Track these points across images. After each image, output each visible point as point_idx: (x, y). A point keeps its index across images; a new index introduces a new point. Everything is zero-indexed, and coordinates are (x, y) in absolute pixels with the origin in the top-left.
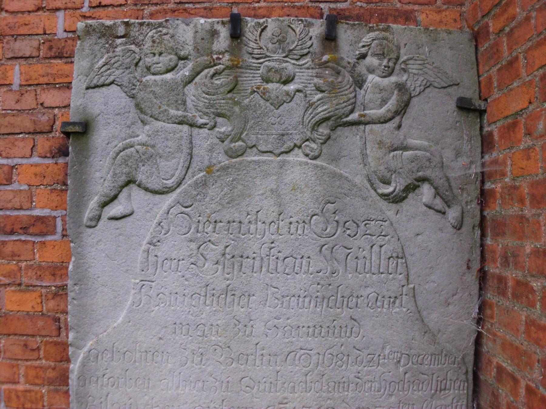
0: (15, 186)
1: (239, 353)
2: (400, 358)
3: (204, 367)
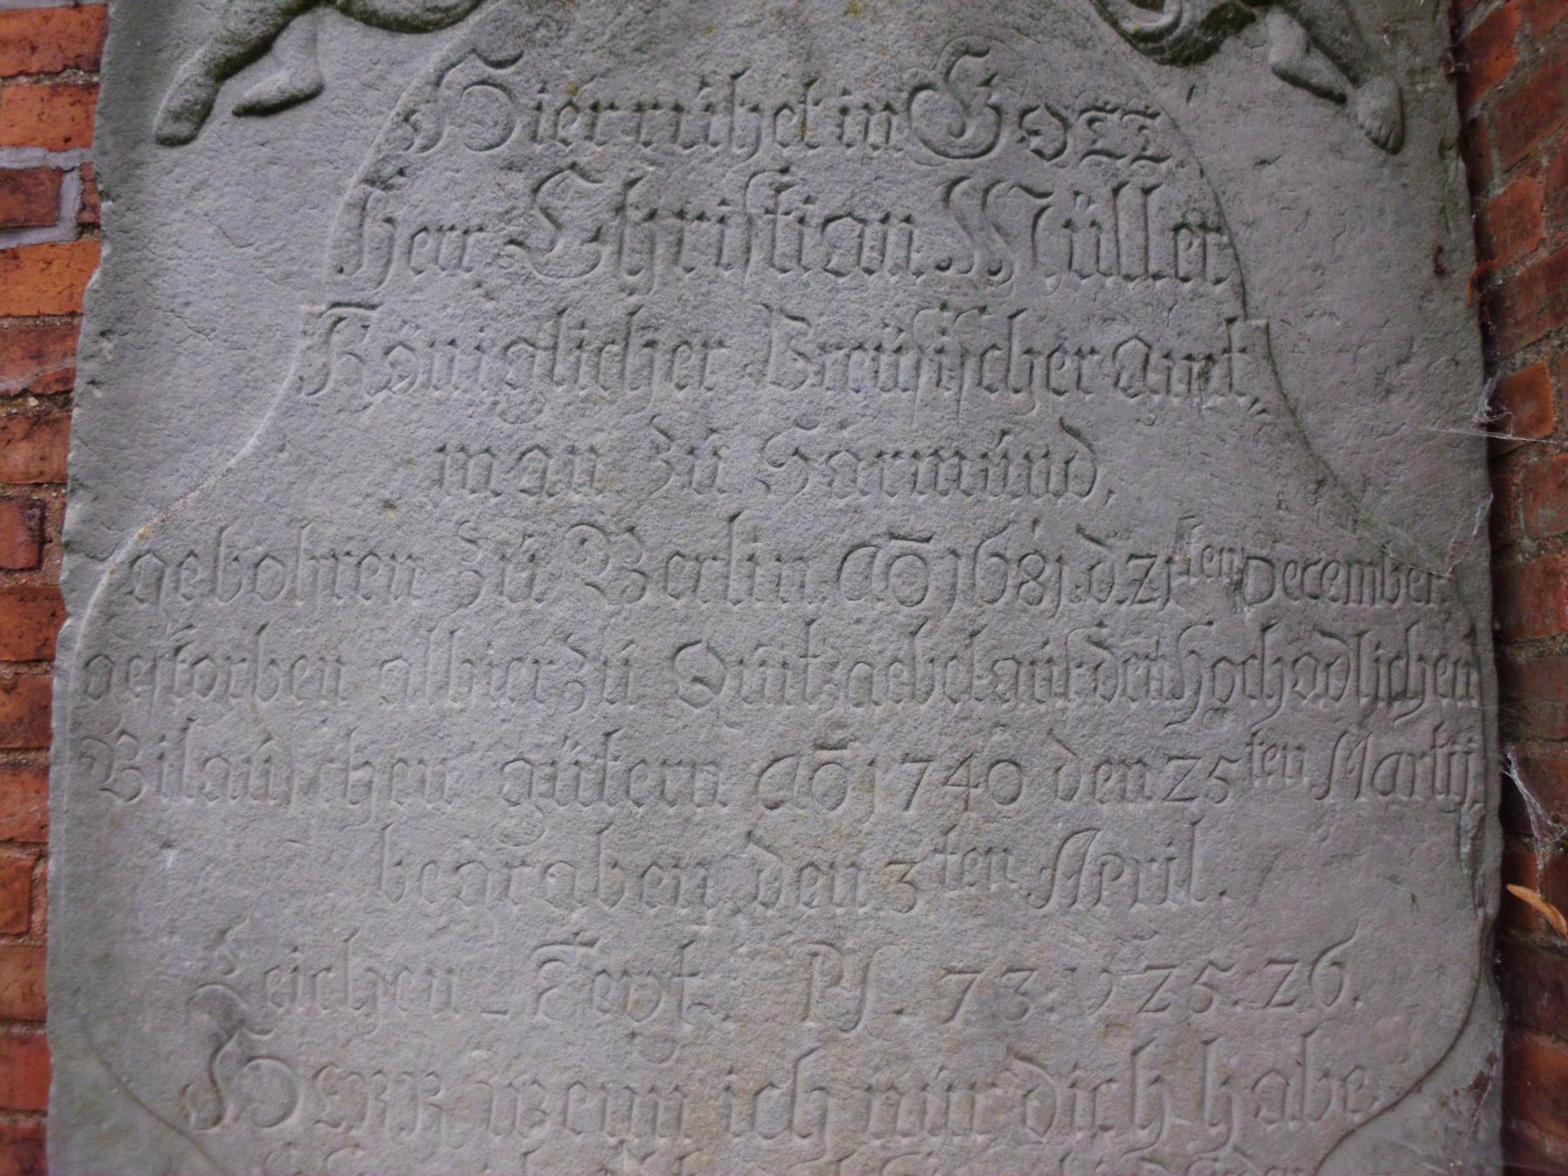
1: (666, 551)
2: (1242, 571)
3: (539, 606)
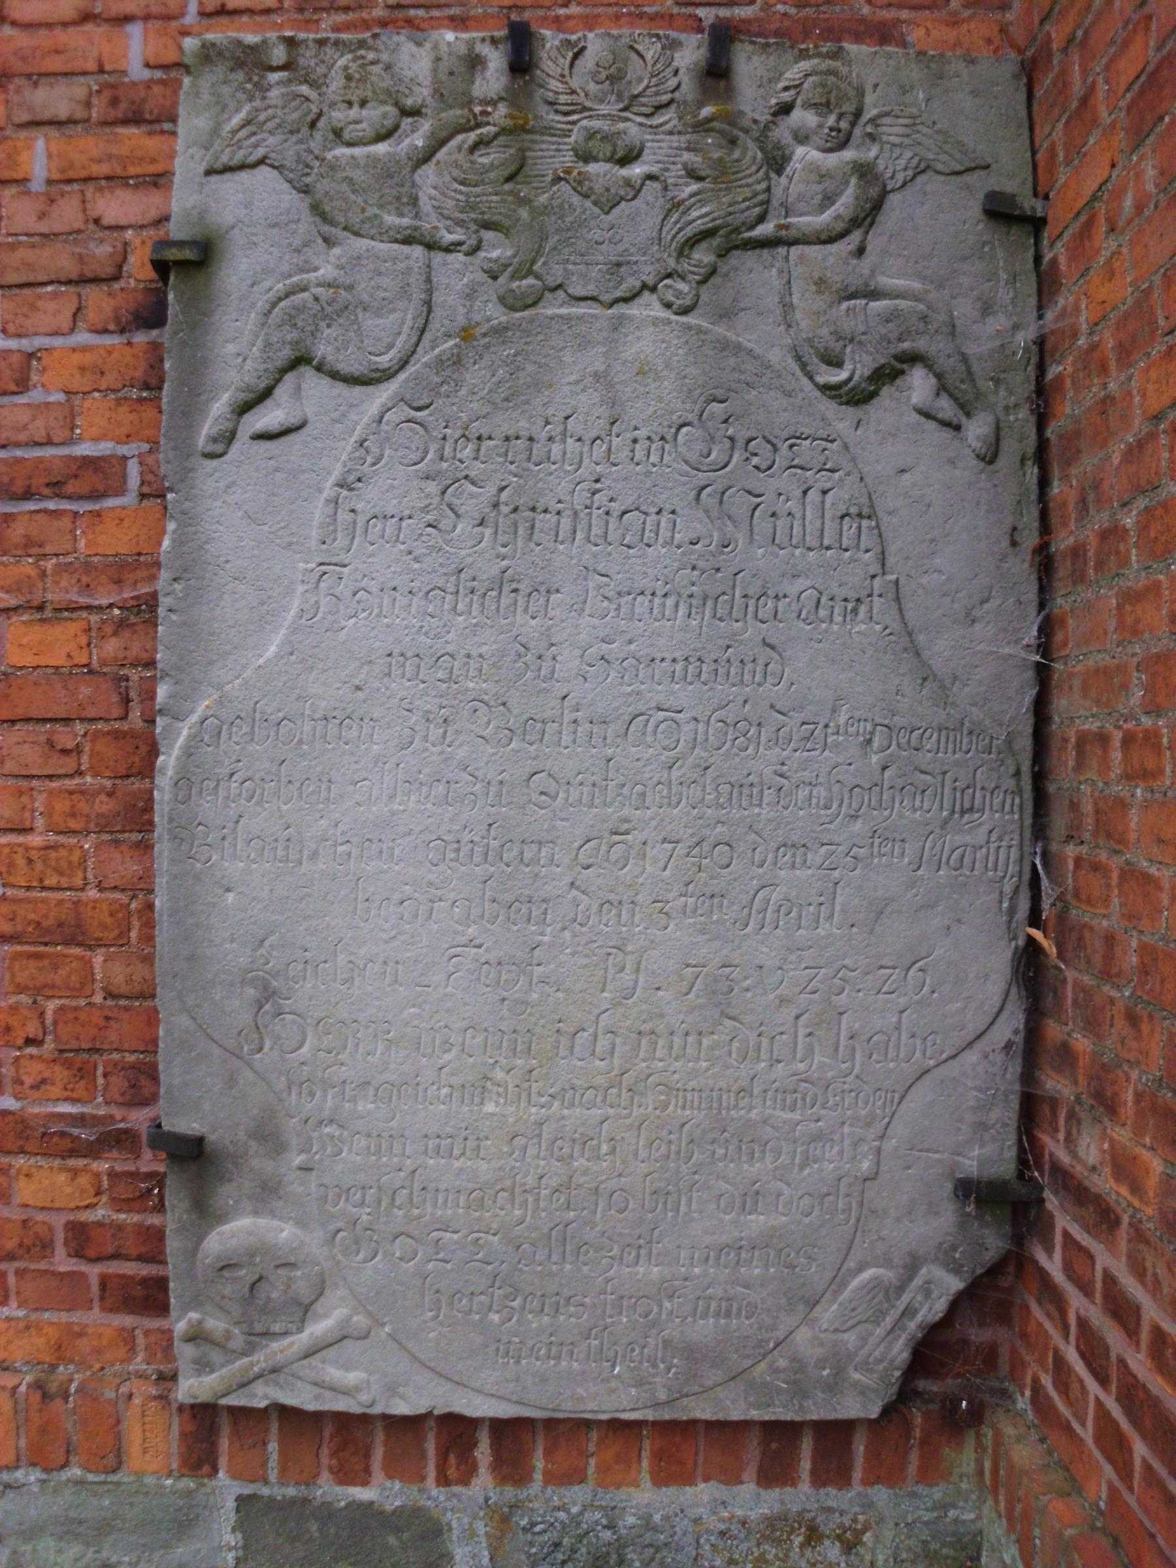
0: (36, 395)
1: (525, 717)
2: (872, 733)
